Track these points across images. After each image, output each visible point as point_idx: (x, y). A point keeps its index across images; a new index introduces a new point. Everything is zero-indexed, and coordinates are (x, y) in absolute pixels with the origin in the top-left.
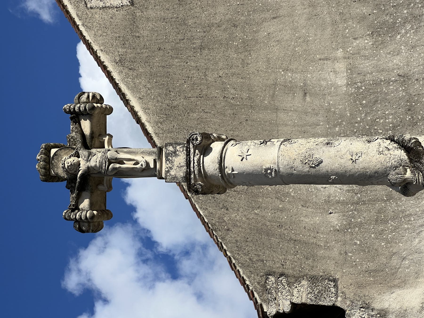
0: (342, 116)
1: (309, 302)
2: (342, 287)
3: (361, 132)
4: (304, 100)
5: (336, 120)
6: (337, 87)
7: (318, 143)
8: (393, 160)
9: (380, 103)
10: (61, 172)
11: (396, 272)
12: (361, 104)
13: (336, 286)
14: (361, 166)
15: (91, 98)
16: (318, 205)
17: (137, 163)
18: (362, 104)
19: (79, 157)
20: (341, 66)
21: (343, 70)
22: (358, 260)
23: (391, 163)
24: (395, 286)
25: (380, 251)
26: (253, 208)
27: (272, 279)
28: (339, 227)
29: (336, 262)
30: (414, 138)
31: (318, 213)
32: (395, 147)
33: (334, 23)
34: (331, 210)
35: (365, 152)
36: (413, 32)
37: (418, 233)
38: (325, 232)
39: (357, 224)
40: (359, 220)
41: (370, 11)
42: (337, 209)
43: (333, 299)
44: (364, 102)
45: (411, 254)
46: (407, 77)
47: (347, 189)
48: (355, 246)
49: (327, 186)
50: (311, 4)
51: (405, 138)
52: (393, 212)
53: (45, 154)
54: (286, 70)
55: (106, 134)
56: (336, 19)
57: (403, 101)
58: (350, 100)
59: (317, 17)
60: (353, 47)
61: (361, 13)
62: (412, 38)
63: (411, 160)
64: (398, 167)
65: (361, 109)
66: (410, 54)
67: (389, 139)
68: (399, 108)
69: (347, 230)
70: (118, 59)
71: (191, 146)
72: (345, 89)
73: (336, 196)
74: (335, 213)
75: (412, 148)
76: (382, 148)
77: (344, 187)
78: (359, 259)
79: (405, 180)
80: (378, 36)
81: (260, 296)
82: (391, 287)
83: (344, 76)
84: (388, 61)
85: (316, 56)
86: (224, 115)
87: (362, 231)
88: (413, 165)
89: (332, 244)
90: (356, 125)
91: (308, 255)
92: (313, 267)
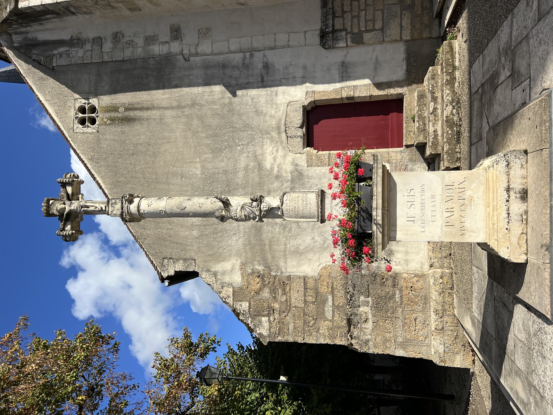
0: (199, 187)
1: (183, 270)
4: (182, 180)
6: (197, 175)
10: (55, 212)
15: (72, 176)
17: (96, 208)
19: (65, 204)
20: (198, 165)
24: (221, 261)
26: (157, 228)
27: (166, 260)
33: (195, 146)
41: (211, 143)
53: (46, 203)
54: (173, 166)
55: (80, 193)
63: (225, 207)
70: (90, 158)
71: (124, 200)
81: (160, 269)
86: (144, 186)
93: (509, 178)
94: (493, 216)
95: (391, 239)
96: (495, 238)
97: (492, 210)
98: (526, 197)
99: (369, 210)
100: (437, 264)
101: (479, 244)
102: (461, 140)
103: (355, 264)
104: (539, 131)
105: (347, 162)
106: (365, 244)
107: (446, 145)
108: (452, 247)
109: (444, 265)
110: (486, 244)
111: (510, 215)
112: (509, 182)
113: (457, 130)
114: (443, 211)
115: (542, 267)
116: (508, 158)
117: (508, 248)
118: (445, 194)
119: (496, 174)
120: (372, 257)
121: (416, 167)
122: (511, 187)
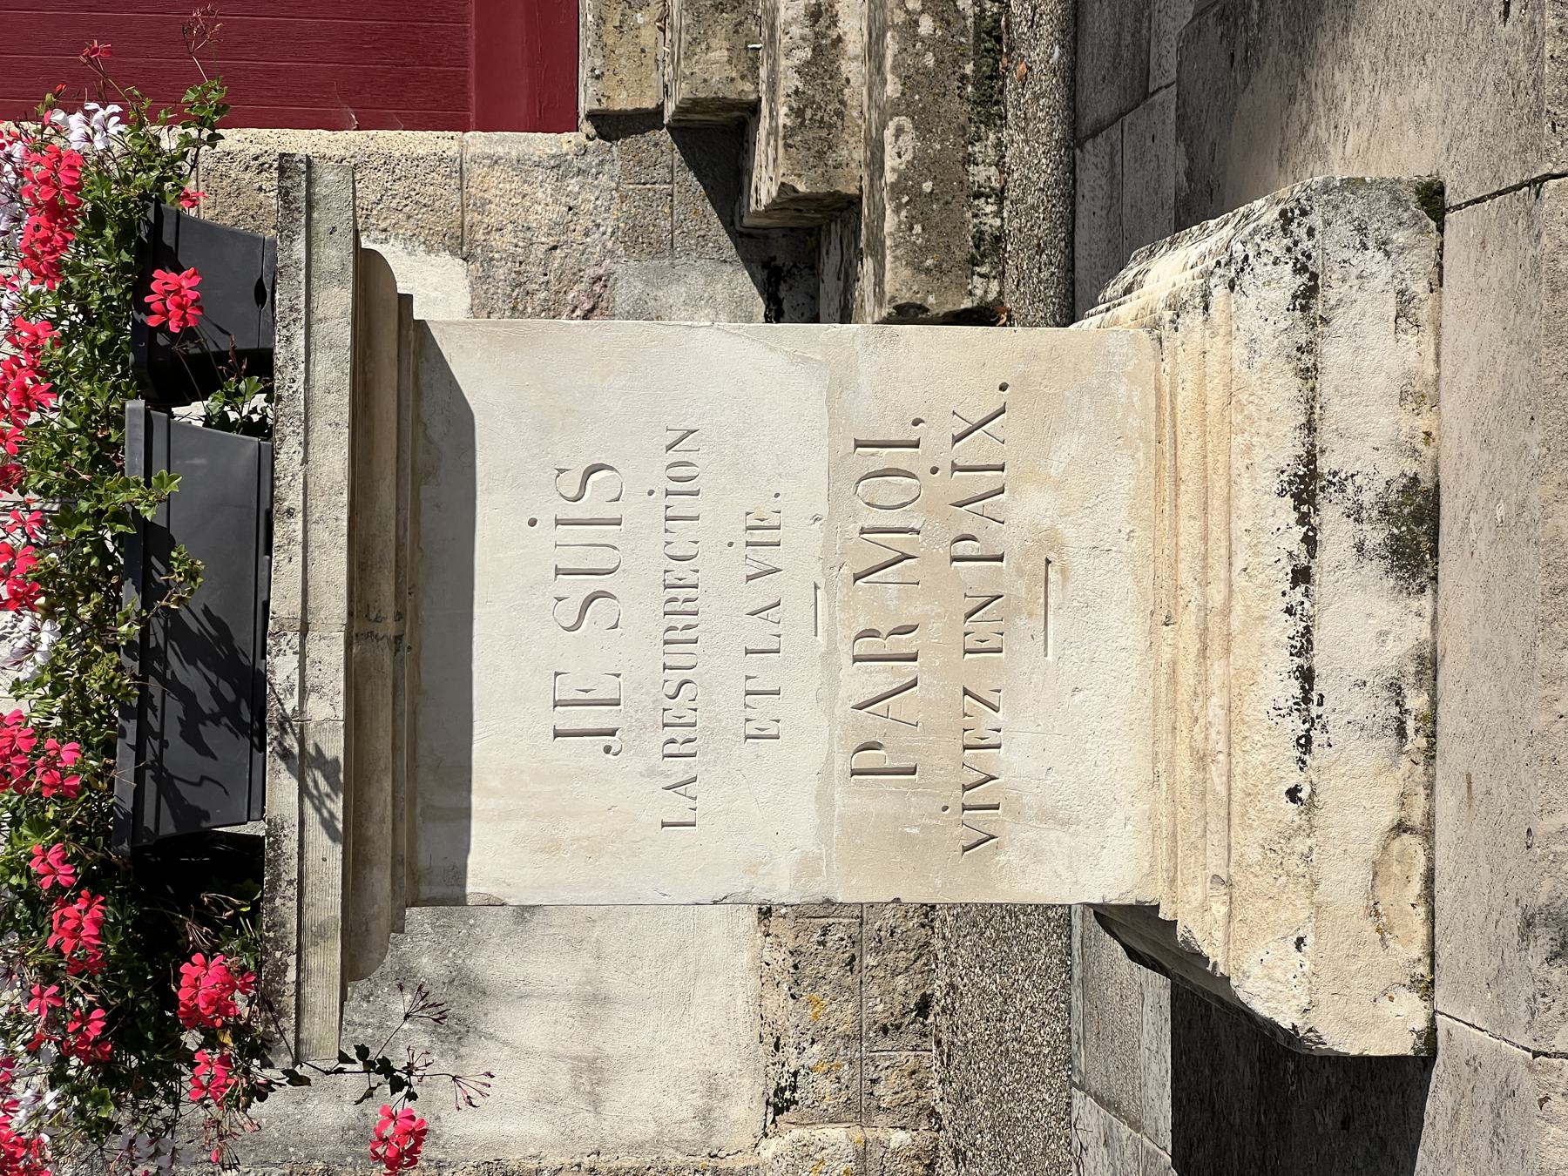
93: (1311, 401)
94: (1200, 693)
95: (425, 891)
96: (1216, 865)
97: (1194, 648)
98: (1425, 544)
99: (243, 638)
100: (826, 1086)
101: (1107, 917)
102: (1011, 97)
103: (108, 1112)
104: (1525, 40)
105: (54, 211)
106: (195, 933)
107: (899, 131)
108: (937, 943)
109: (879, 1090)
110: (1145, 914)
111: (1319, 686)
112: (1310, 427)
113: (980, 17)
114: (832, 650)
115: (1528, 1086)
116: (1306, 244)
117: (1300, 942)
118: (854, 514)
119: (1227, 360)
120: (258, 1049)
121: (675, 294)
122: (1325, 465)
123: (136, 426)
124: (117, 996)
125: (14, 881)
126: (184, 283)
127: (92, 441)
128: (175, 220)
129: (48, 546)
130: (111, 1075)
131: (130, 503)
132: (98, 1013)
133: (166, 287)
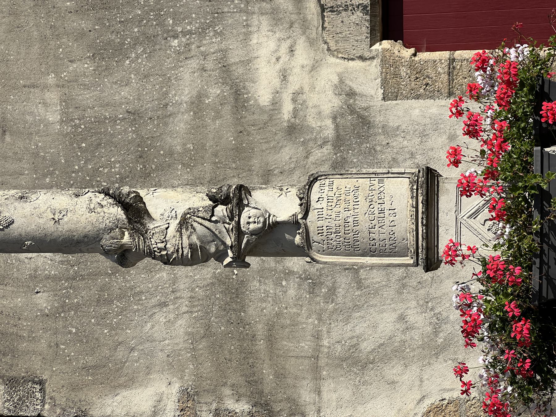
0: (54, 163)
2: (51, 390)
3: (79, 184)
5: (47, 167)
6: (47, 124)
7: (8, 196)
8: (107, 221)
9: (105, 147)
11: (122, 368)
12: (79, 148)
13: (42, 390)
14: (66, 227)
16: (20, 282)
18: (81, 148)
20: (53, 96)
21: (56, 102)
22: (73, 354)
23: (104, 224)
25: (102, 341)
28: (49, 310)
29: (43, 358)
30: (134, 192)
31: (20, 292)
32: (110, 203)
33: (43, 39)
34: (38, 288)
35: (71, 209)
36: (146, 57)
37: (151, 315)
38: (30, 317)
39: (73, 306)
40: (76, 300)
41: (90, 27)
42: (46, 287)
43: (39, 407)
44: (84, 145)
45: (141, 343)
46: (138, 114)
47: (60, 259)
48: (69, 336)
49: (34, 255)
50: (12, 12)
51: (123, 191)
52: (120, 289)
56: (45, 34)
57: (133, 145)
58: (65, 142)
59: (20, 29)
60: (68, 72)
61: (79, 28)
62: (144, 64)
63: (130, 220)
64: (113, 229)
65: (79, 154)
66: (142, 85)
67: (103, 193)
68: (128, 155)
69: (59, 314)
72: (59, 127)
73: (45, 270)
74: (43, 292)
75: (131, 205)
76: (93, 204)
77: (56, 257)
78: (75, 353)
79: (122, 245)
80: (101, 60)
82: (115, 387)
83: (57, 110)
84: (114, 93)
85: (19, 82)
87: (79, 314)
88: (132, 226)
89: (38, 334)
90: (73, 175)
91: (6, 350)
92: (12, 365)
123: (537, 156)
124: (534, 354)
125: (498, 313)
126: (554, 106)
127: (522, 161)
128: (548, 83)
129: (507, 198)
130: (531, 381)
131: (536, 183)
132: (528, 360)
133: (547, 108)
